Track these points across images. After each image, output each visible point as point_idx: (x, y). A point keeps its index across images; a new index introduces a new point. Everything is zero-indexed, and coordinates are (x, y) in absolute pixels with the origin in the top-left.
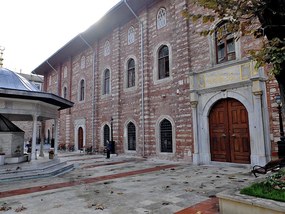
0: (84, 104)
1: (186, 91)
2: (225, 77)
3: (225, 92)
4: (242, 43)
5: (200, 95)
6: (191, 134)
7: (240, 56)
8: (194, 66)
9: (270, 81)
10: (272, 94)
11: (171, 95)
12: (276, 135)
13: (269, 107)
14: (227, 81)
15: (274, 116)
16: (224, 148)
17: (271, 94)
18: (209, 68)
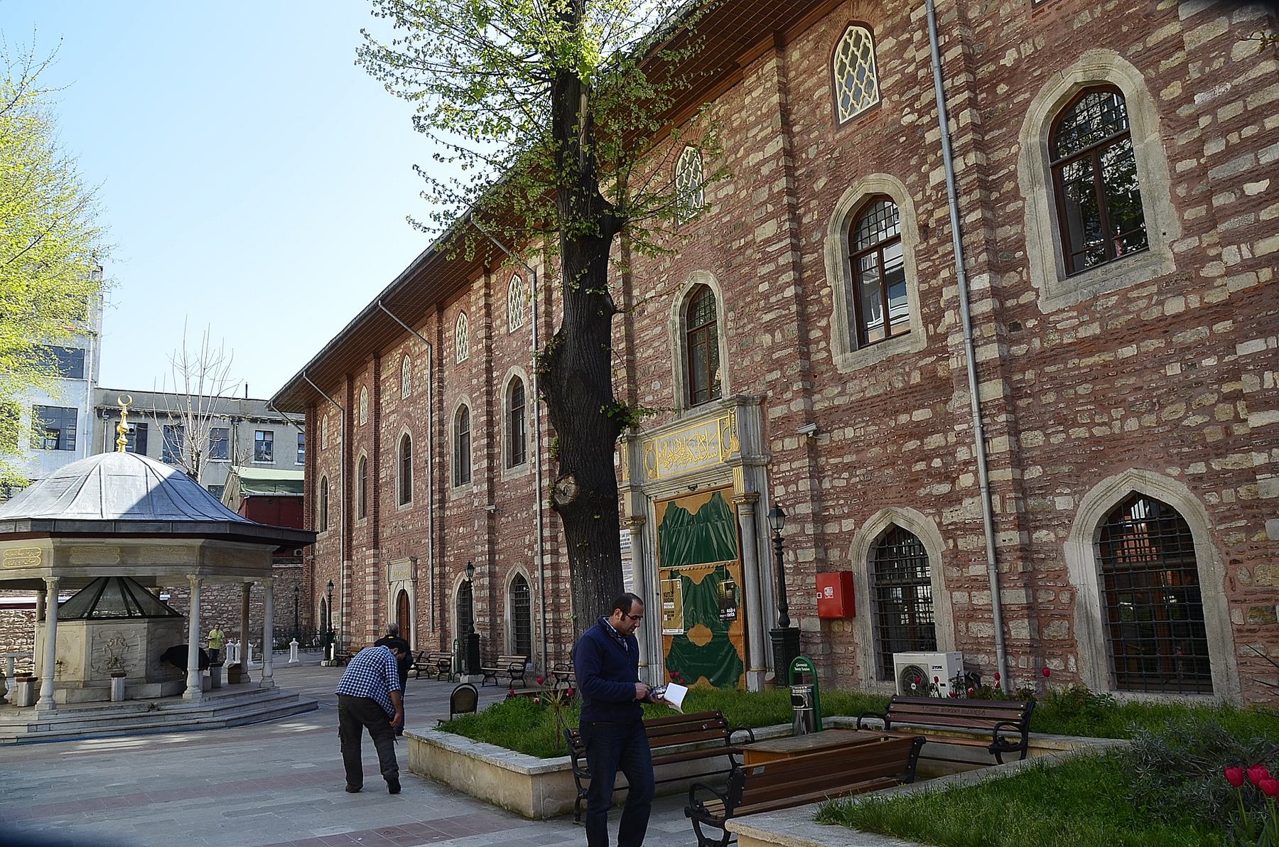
0: (412, 513)
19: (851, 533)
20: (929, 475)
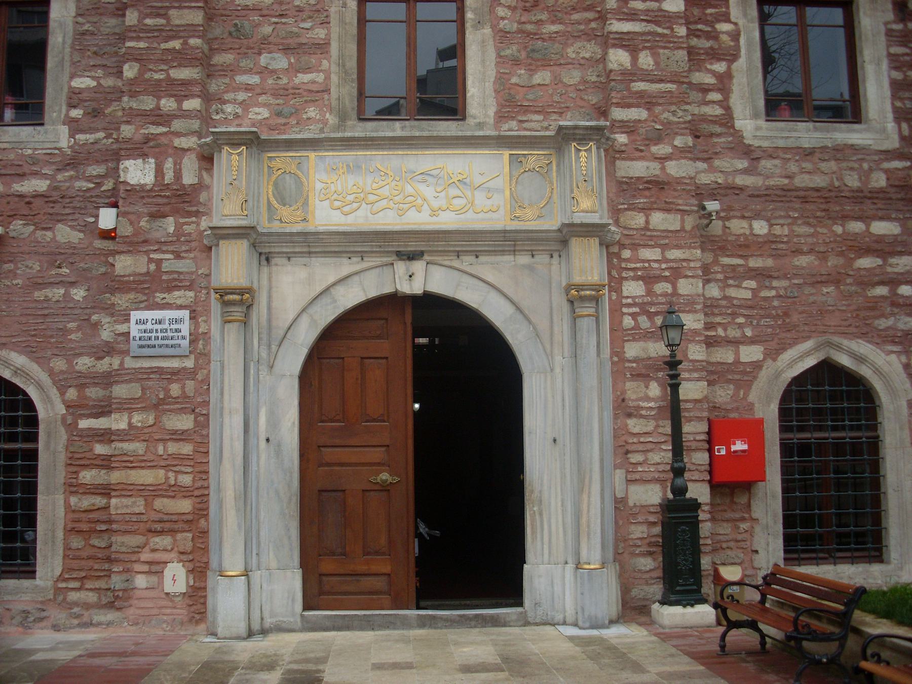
1: (170, 225)
2: (428, 191)
3: (418, 266)
4: (501, 57)
5: (268, 260)
6: (189, 470)
7: (491, 112)
8: (226, 97)
9: (622, 246)
10: (629, 305)
11: (49, 234)
12: (637, 476)
13: (616, 359)
14: (434, 212)
15: (634, 397)
16: (383, 541)
17: (624, 301)
18: (322, 130)
19: (757, 366)
20: (893, 304)
